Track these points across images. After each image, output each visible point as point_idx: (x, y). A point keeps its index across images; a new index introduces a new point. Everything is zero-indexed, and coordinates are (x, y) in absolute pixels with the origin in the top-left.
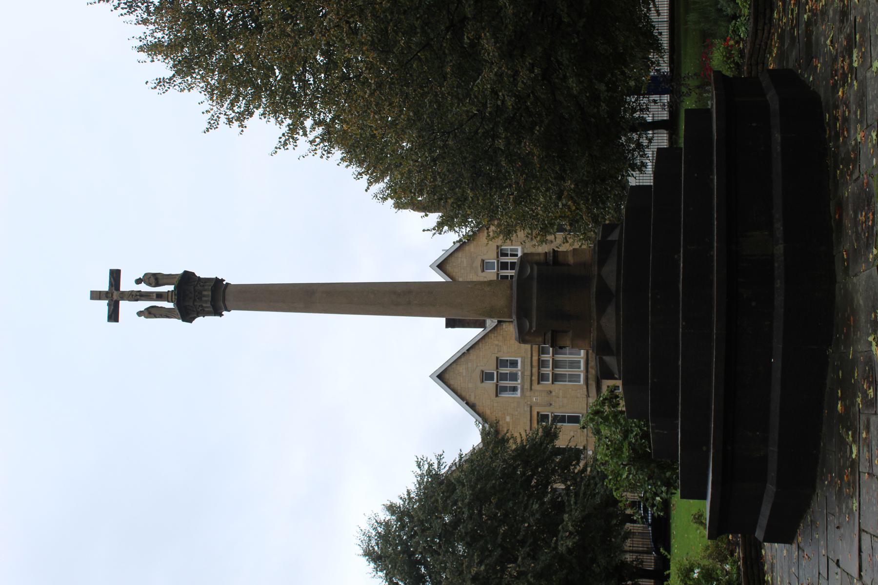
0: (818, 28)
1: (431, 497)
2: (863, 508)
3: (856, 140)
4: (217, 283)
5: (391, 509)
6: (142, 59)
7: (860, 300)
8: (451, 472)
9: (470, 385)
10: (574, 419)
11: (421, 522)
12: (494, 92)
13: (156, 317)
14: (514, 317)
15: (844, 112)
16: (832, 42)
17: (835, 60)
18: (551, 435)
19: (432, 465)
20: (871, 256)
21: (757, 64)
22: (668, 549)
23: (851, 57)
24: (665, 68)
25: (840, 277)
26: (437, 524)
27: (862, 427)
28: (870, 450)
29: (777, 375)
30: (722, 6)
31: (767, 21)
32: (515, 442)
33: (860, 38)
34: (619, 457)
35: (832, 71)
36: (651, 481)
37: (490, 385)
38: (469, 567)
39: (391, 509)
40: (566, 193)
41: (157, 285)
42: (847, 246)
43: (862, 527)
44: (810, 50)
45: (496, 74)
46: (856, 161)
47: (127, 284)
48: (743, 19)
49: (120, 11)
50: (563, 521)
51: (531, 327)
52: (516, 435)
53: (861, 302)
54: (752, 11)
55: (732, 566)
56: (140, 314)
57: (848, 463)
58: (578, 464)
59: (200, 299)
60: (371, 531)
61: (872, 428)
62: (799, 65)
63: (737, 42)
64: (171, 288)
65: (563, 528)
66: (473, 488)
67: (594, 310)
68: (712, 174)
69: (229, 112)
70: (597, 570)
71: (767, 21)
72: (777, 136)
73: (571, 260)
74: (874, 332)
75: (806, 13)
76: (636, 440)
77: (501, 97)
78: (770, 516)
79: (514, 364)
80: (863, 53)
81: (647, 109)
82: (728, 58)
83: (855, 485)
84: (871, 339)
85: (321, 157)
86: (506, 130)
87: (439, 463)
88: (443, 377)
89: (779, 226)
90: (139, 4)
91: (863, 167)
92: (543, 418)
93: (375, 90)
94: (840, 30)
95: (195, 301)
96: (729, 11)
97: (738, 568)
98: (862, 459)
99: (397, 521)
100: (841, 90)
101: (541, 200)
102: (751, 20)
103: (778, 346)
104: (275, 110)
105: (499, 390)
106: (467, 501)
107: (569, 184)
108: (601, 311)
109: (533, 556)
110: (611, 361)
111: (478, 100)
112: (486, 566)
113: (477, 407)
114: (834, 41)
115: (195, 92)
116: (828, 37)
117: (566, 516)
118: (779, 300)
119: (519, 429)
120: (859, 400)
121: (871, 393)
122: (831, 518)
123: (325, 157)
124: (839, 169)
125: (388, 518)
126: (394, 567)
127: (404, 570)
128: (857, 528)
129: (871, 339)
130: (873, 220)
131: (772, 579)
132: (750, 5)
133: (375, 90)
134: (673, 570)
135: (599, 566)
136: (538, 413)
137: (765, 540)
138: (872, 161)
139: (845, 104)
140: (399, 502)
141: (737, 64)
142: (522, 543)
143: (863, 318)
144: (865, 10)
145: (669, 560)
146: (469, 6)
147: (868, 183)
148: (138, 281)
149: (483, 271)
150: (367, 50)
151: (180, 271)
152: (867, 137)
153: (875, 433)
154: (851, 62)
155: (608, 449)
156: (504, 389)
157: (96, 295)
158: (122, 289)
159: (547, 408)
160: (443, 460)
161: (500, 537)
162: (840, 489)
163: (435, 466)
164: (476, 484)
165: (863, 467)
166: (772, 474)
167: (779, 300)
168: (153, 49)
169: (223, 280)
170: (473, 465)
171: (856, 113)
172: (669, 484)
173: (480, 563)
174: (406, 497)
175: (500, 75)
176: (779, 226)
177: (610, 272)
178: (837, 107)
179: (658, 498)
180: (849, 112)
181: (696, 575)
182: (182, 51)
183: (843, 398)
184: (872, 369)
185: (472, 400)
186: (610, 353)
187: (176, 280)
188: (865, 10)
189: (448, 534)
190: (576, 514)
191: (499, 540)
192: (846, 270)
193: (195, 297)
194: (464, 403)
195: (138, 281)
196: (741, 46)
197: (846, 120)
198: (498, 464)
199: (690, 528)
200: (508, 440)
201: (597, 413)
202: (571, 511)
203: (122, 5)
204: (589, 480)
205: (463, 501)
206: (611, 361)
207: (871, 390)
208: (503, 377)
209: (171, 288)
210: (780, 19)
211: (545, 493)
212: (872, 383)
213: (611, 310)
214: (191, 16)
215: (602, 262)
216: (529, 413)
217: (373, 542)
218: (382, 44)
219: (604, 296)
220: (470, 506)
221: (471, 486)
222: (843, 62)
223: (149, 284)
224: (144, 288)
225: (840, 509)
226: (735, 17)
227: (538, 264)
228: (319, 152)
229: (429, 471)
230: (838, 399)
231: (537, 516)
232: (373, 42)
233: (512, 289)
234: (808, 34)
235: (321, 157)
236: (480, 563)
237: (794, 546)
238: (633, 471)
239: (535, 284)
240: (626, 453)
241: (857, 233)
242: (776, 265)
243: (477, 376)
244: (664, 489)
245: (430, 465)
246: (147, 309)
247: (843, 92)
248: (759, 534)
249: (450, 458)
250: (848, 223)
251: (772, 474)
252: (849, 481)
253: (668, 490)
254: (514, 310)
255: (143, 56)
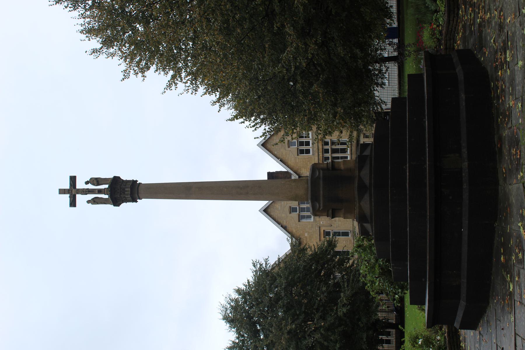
0: (486, 30)
1: (262, 284)
2: (517, 321)
3: (509, 104)
4: (134, 183)
5: (238, 291)
6: (83, 39)
7: (513, 200)
8: (273, 268)
9: (283, 215)
10: (346, 234)
11: (257, 299)
12: (295, 58)
13: (98, 204)
14: (310, 201)
15: (502, 85)
16: (494, 41)
17: (496, 52)
18: (332, 244)
19: (262, 265)
20: (519, 176)
21: (450, 40)
22: (403, 326)
23: (505, 54)
24: (395, 25)
25: (501, 182)
26: (266, 300)
27: (515, 274)
28: (520, 289)
29: (465, 238)
30: (429, 5)
31: (455, 15)
32: (311, 249)
33: (511, 44)
34: (374, 272)
35: (494, 58)
36: (392, 286)
37: (295, 215)
38: (286, 325)
39: (238, 291)
40: (338, 115)
41: (98, 184)
42: (505, 166)
43: (517, 332)
44: (481, 42)
45: (295, 49)
46: (510, 116)
47: (80, 185)
48: (441, 13)
49: (68, 9)
50: (341, 297)
51: (320, 207)
52: (311, 244)
53: (514, 201)
54: (446, 9)
55: (441, 336)
56: (88, 202)
57: (508, 293)
58: (348, 262)
59: (124, 193)
60: (227, 305)
61: (521, 276)
62: (475, 48)
63: (438, 26)
64: (106, 186)
65: (340, 301)
66: (287, 278)
67: (357, 196)
68: (425, 118)
69: (136, 68)
70: (362, 325)
71: (455, 15)
72: (463, 96)
73: (342, 167)
74: (522, 221)
75: (478, 18)
76: (383, 263)
77: (299, 60)
78: (462, 321)
79: (308, 144)
80: (513, 54)
81: (385, 49)
82: (433, 35)
83: (512, 307)
84: (520, 224)
85: (192, 94)
86: (302, 78)
87: (266, 263)
88: (264, 145)
89: (465, 151)
90: (80, 5)
91: (514, 122)
92: (327, 234)
93: (223, 59)
94: (499, 36)
95: (121, 194)
96: (433, 8)
97: (445, 337)
98: (515, 293)
99: (242, 298)
100: (500, 71)
101: (323, 115)
102: (446, 15)
103: (465, 222)
104: (164, 68)
105: (300, 218)
106: (283, 286)
107: (340, 110)
108: (361, 197)
109: (323, 318)
110: (368, 226)
111: (286, 65)
112: (296, 325)
113: (288, 228)
114: (496, 41)
115: (116, 58)
116: (492, 37)
117: (342, 294)
118: (466, 196)
119: (313, 242)
120: (513, 258)
121: (520, 255)
122: (498, 322)
123: (194, 94)
124: (499, 118)
125: (237, 297)
126: (241, 326)
127: (247, 327)
128: (513, 334)
129: (520, 224)
130: (520, 155)
131: (465, 346)
132: (445, 5)
133: (223, 59)
134: (407, 338)
135: (362, 323)
136: (324, 231)
137: (461, 328)
138: (518, 119)
139: (502, 80)
140: (243, 287)
141: (438, 39)
142: (317, 310)
143: (515, 211)
144: (513, 29)
145: (404, 332)
146: (277, 6)
147: (517, 132)
148: (87, 183)
149: (289, 147)
150: (218, 34)
151: (111, 176)
152: (516, 104)
153: (523, 280)
154: (505, 58)
155: (366, 267)
156: (304, 217)
157: (62, 192)
158: (77, 188)
159: (329, 228)
160: (268, 262)
161: (303, 307)
162: (503, 306)
163: (264, 265)
164: (288, 276)
165: (517, 297)
166: (463, 295)
167: (466, 196)
168: (90, 32)
169: (137, 181)
170: (285, 262)
171: (509, 88)
172: (403, 288)
173: (293, 322)
174: (247, 284)
175: (297, 48)
176: (465, 151)
177: (365, 173)
178: (498, 81)
179: (397, 296)
180: (505, 87)
181: (420, 343)
182: (107, 32)
183: (503, 254)
184: (521, 242)
185: (284, 224)
186: (367, 222)
187: (109, 182)
188: (513, 29)
189: (273, 304)
190: (348, 293)
191: (303, 309)
192: (505, 179)
193: (120, 191)
194: (280, 226)
195: (87, 183)
196: (440, 28)
197: (503, 90)
198: (301, 263)
199: (416, 318)
200: (306, 249)
201: (359, 246)
202: (345, 291)
203: (70, 6)
204: (355, 272)
205: (281, 286)
206: (368, 226)
207: (520, 254)
208: (301, 144)
209: (106, 186)
210: (463, 16)
211: (329, 279)
212: (521, 250)
213: (367, 197)
214: (111, 11)
215: (360, 169)
216: (318, 231)
217: (228, 311)
218: (227, 31)
219: (362, 189)
220: (285, 289)
221: (285, 277)
222: (501, 55)
223: (94, 184)
224: (90, 186)
225: (504, 319)
226: (436, 11)
227: (323, 169)
228: (190, 91)
229: (260, 268)
230: (501, 254)
231: (325, 294)
232: (220, 30)
233: (308, 184)
234: (481, 32)
235: (192, 94)
236: (293, 322)
237: (477, 332)
238: (382, 281)
239: (321, 182)
240: (377, 270)
241: (511, 160)
242: (464, 174)
243: (287, 209)
244: (400, 290)
245: (261, 265)
246: (93, 199)
247: (501, 73)
248: (457, 325)
249: (272, 261)
250: (505, 152)
251: (463, 295)
252: (508, 303)
253: (402, 291)
254: (309, 196)
255: (83, 36)
